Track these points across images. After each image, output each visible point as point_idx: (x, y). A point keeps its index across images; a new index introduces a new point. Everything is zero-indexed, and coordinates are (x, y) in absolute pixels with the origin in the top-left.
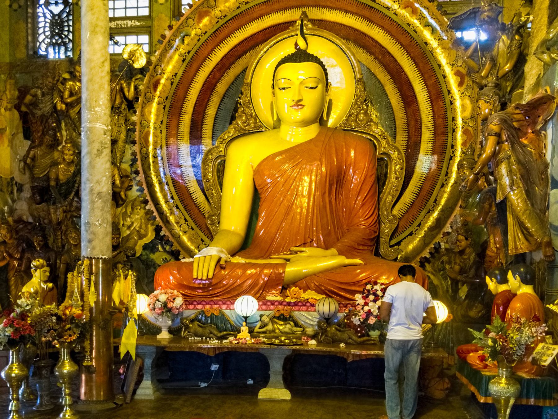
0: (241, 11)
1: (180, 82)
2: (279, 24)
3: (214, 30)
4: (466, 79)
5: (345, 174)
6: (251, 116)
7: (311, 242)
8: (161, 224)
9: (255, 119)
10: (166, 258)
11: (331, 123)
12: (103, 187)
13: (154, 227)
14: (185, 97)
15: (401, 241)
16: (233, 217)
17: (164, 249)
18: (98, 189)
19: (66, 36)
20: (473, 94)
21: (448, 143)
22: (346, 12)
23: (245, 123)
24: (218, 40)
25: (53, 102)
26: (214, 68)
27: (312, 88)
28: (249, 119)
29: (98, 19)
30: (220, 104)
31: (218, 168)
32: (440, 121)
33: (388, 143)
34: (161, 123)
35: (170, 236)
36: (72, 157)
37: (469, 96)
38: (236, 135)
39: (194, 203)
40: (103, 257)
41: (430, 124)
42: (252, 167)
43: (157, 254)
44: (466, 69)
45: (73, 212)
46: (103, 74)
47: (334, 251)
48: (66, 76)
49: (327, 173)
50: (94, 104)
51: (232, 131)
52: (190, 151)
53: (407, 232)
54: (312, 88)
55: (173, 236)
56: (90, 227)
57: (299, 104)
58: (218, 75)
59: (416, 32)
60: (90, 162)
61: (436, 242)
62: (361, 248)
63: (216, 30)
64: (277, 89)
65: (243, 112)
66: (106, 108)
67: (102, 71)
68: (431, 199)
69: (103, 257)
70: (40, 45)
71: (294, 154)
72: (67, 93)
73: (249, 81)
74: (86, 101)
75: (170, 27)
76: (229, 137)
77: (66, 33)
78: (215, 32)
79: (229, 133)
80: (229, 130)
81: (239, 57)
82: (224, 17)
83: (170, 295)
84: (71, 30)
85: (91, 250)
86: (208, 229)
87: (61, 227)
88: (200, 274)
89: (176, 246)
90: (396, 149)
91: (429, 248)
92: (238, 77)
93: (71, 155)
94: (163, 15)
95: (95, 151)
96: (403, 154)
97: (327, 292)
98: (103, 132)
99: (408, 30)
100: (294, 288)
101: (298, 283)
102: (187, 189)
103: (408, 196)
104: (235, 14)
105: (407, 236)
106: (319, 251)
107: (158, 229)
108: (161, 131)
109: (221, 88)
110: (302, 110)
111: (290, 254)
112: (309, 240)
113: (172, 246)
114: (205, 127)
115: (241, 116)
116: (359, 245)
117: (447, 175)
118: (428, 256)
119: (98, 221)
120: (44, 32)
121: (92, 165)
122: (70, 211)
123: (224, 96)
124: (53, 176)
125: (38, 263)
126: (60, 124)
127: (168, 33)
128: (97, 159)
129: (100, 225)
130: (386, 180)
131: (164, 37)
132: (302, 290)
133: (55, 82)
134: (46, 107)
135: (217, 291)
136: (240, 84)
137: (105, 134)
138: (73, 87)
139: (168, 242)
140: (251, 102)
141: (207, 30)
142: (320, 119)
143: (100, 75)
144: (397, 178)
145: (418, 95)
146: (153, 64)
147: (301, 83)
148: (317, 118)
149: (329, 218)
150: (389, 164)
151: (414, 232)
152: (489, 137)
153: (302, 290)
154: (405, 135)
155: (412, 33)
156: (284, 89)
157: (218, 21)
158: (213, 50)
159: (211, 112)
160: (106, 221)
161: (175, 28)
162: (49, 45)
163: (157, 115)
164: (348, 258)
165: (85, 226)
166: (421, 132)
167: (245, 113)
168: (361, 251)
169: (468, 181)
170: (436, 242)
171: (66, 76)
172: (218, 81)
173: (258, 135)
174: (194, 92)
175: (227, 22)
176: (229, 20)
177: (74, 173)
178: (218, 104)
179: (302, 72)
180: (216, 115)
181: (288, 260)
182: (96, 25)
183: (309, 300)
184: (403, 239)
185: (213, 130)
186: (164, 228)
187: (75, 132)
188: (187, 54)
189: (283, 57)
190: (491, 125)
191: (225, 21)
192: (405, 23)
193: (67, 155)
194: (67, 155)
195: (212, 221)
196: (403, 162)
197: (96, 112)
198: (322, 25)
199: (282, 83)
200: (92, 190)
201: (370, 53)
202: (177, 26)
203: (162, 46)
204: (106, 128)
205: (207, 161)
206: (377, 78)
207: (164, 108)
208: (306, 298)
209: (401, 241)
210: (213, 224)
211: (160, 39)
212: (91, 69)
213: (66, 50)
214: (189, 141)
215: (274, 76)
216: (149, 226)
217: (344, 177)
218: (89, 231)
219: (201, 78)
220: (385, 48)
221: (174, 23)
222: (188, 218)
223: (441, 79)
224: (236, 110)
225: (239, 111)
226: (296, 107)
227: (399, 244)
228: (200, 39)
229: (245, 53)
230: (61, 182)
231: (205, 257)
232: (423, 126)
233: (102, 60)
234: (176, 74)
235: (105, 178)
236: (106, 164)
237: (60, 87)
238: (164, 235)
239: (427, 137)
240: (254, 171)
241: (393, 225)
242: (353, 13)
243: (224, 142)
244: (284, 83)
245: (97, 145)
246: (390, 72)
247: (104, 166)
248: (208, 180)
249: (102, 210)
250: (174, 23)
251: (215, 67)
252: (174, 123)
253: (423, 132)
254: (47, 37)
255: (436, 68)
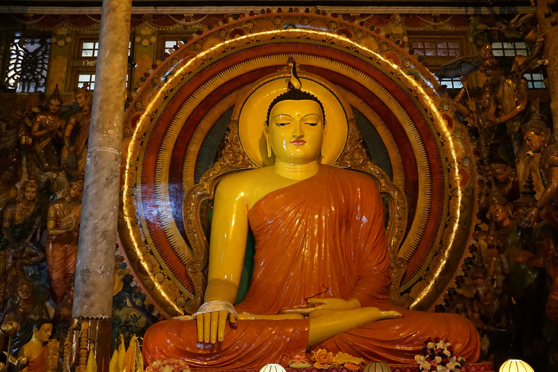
0: (227, 55)
1: (161, 118)
2: (266, 68)
3: (198, 71)
4: (454, 122)
5: (352, 213)
6: (239, 152)
7: (326, 292)
8: (132, 273)
9: (244, 156)
10: (135, 315)
11: (324, 161)
12: (109, 225)
13: (122, 276)
14: (165, 134)
15: (411, 287)
16: (227, 262)
17: (133, 303)
18: (103, 226)
19: (40, 73)
20: (463, 136)
21: (446, 183)
22: (332, 59)
23: (233, 160)
24: (203, 79)
25: (18, 136)
26: (198, 106)
27: (312, 125)
28: (236, 156)
29: (119, 39)
30: (204, 141)
31: (201, 208)
32: (433, 161)
33: (386, 182)
34: (138, 160)
35: (142, 287)
36: (34, 195)
37: (459, 138)
38: (221, 173)
39: (172, 247)
40: (104, 317)
41: (425, 164)
42: (247, 207)
43: (124, 310)
44: (453, 113)
45: (23, 259)
46: (120, 94)
47: (354, 302)
48: (36, 110)
49: (336, 212)
50: (107, 126)
51: (218, 169)
52: (169, 190)
53: (416, 277)
54: (312, 125)
55: (146, 287)
56: (89, 276)
57: (299, 141)
58: (202, 112)
59: (400, 80)
60: (96, 194)
61: (450, 288)
62: (381, 297)
63: (202, 71)
64: (273, 125)
65: (230, 149)
66: (120, 131)
67: (119, 91)
68: (436, 240)
69: (104, 317)
70: (8, 80)
71: (296, 192)
72: (36, 126)
73: (236, 118)
74: (98, 122)
75: (154, 66)
76: (214, 174)
77: (39, 70)
78: (200, 72)
79: (215, 170)
80: (215, 167)
81: (225, 96)
82: (210, 59)
83: (176, 366)
84: (46, 66)
85: (88, 308)
86: (188, 277)
87: (6, 279)
88: (207, 337)
89: (149, 300)
90: (396, 188)
91: (443, 294)
92: (223, 114)
93: (33, 192)
94: (146, 56)
95: (103, 180)
96: (403, 192)
97: (364, 353)
98: (114, 158)
99: (392, 77)
100: (320, 350)
101: (323, 344)
102: (164, 232)
103: (412, 238)
104: (220, 57)
105: (416, 282)
106: (338, 303)
107: (127, 280)
108: (137, 168)
109: (205, 125)
110: (304, 146)
111: (307, 307)
112: (324, 290)
113: (144, 300)
114: (186, 164)
115: (228, 153)
116: (378, 293)
117: (448, 215)
118: (444, 304)
119: (101, 268)
120: (15, 69)
121: (98, 197)
122: (20, 258)
123: (208, 132)
124: (8, 215)
125: (10, 327)
126: (21, 159)
127: (151, 71)
128: (106, 190)
129: (103, 273)
130: (388, 220)
131: (147, 75)
132: (331, 353)
133: (24, 115)
134: (9, 140)
135: (226, 358)
136: (227, 122)
137: (116, 160)
138: (43, 121)
139: (139, 295)
140: (238, 139)
141: (192, 70)
142: (317, 156)
143: (117, 94)
144: (400, 219)
145: (409, 136)
146: (133, 101)
147: (302, 119)
148: (315, 156)
149: (341, 263)
150: (390, 203)
151: (423, 277)
152: (553, 168)
153: (331, 353)
154: (402, 174)
155: (397, 81)
156: (283, 125)
157: (203, 63)
158: (197, 88)
159: (194, 148)
160: (109, 269)
161: (159, 67)
162: (17, 81)
163: (134, 153)
164: (382, 309)
165: (83, 275)
166: (417, 172)
167: (233, 151)
168: (382, 301)
169: (531, 216)
170: (450, 288)
171: (36, 110)
172: (202, 118)
173: (248, 172)
174: (175, 128)
175: (213, 63)
176: (215, 62)
177: (33, 214)
178: (202, 140)
179: (295, 110)
180: (199, 151)
181: (307, 315)
182: (118, 45)
183: (346, 366)
184: (413, 285)
185: (196, 167)
186: (135, 278)
187: (39, 168)
188: (169, 92)
189: (279, 95)
190: (552, 156)
191: (210, 63)
192: (389, 71)
193: (28, 192)
194: (28, 192)
195: (194, 269)
196: (405, 201)
197: (109, 135)
198: (310, 69)
199: (281, 119)
200: (95, 228)
201: (359, 96)
202: (162, 66)
203: (144, 84)
204: (117, 153)
205: (189, 200)
206: (367, 119)
207: (141, 144)
208: (340, 363)
209: (411, 287)
210: (196, 272)
211: (144, 76)
212: (107, 89)
213: (38, 86)
214: (168, 178)
215: (269, 114)
216: (116, 275)
217: (351, 217)
218: (88, 282)
219: (184, 115)
220: (372, 92)
221: (158, 62)
222: (164, 265)
223: (430, 122)
224: (222, 146)
225: (226, 148)
226: (297, 144)
227: (408, 291)
228: (184, 78)
229: (231, 92)
230: (17, 223)
231: (211, 313)
232: (418, 166)
233: (120, 79)
234: (157, 110)
235: (112, 213)
236: (114, 196)
237: (27, 121)
238: (136, 287)
239: (423, 177)
240: (249, 212)
241: (402, 270)
242: (338, 61)
243: (209, 180)
244: (283, 119)
245: (106, 173)
246: (379, 114)
247: (112, 199)
248: (190, 222)
249: (106, 254)
250: (158, 62)
251: (199, 104)
252: (152, 158)
253: (419, 172)
254: (17, 73)
255: (423, 112)
